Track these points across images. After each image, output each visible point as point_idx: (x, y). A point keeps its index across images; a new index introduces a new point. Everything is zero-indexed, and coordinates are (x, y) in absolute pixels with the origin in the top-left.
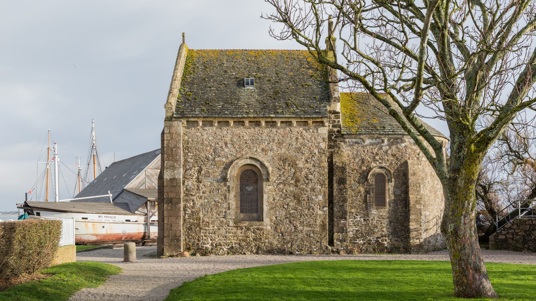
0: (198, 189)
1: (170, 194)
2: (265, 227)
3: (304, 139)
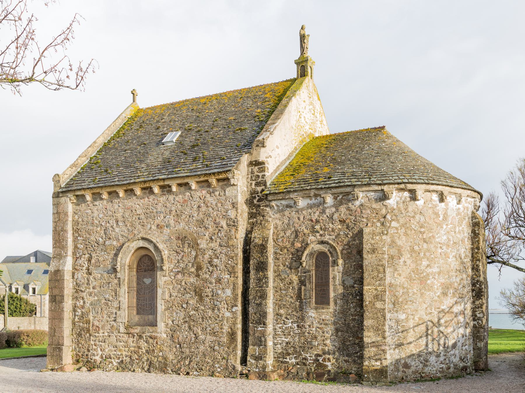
0: (88, 284)
1: (54, 291)
2: (159, 335)
3: (207, 207)
